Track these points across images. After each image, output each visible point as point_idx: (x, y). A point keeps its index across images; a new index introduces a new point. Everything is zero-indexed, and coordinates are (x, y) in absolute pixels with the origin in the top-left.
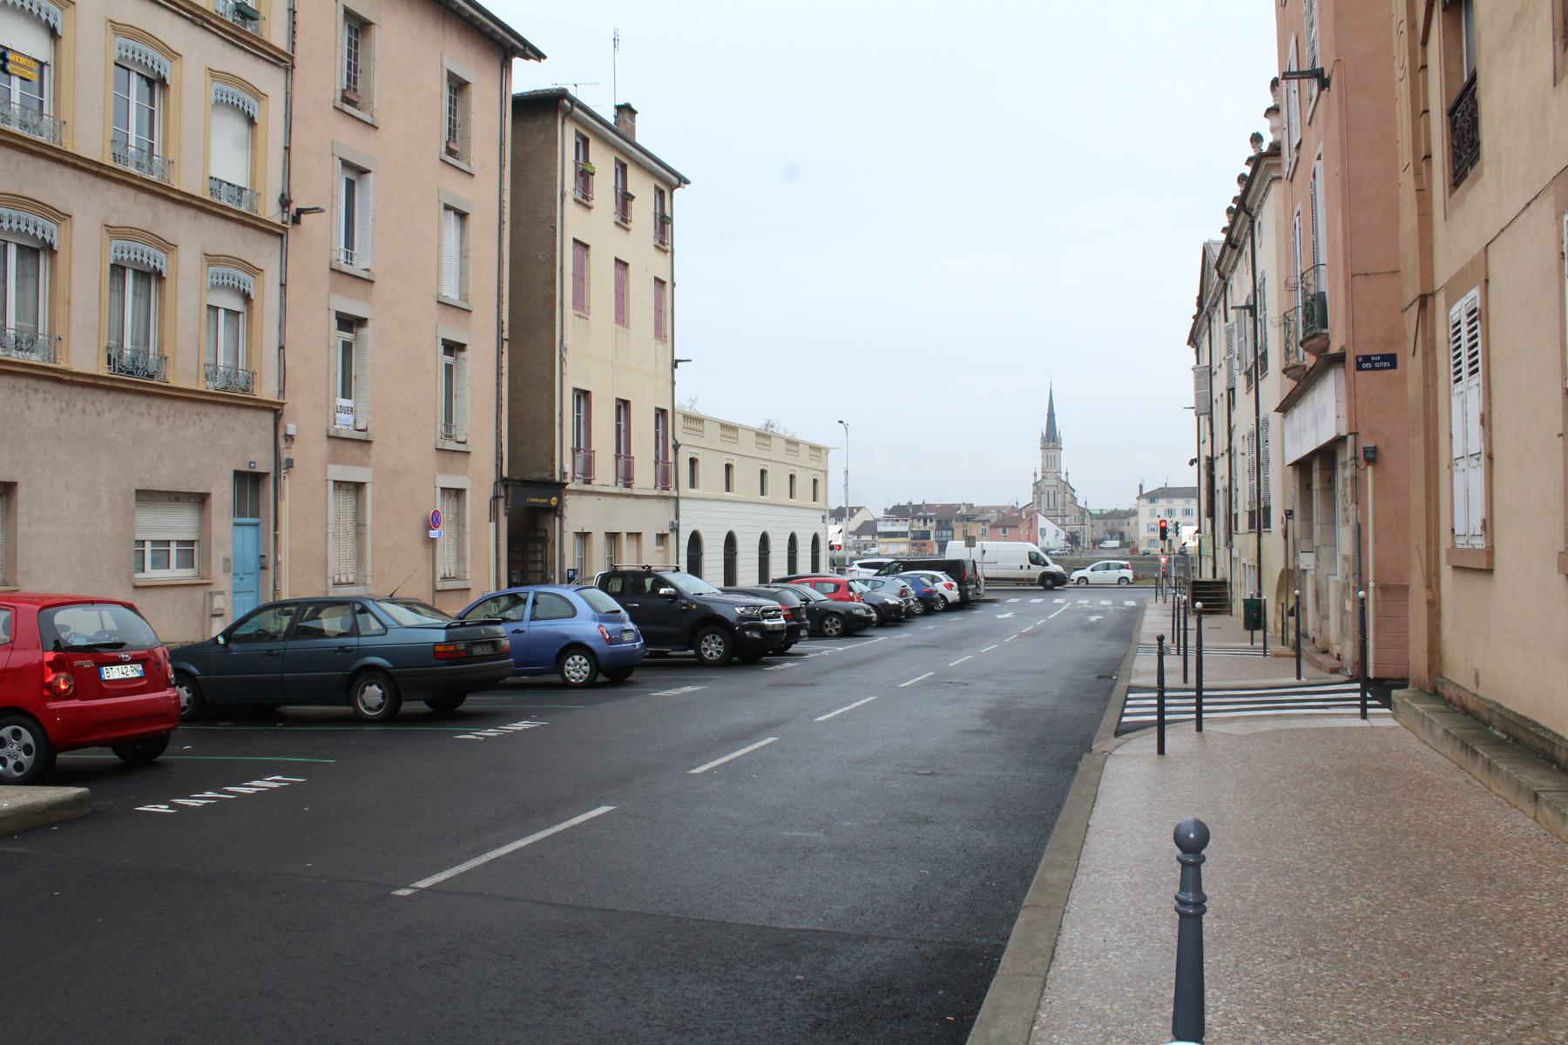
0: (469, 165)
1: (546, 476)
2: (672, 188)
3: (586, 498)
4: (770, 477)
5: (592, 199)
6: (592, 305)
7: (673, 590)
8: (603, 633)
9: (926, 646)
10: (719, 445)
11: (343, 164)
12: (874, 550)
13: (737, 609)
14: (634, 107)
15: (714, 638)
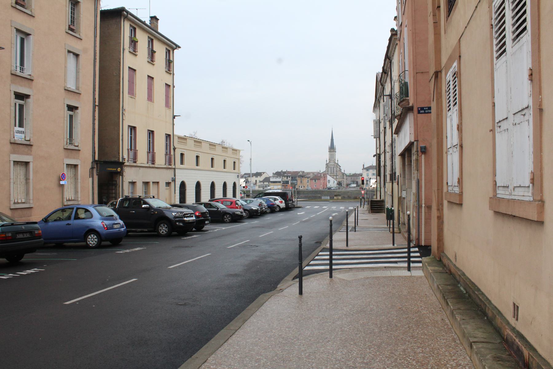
0: (80, 35)
1: (116, 160)
2: (173, 49)
3: (133, 169)
4: (215, 161)
5: (137, 52)
6: (137, 93)
7: (148, 205)
8: (103, 225)
9: (259, 227)
10: (194, 149)
11: (16, 30)
12: (269, 188)
13: (173, 213)
14: (158, 17)
15: (164, 225)
